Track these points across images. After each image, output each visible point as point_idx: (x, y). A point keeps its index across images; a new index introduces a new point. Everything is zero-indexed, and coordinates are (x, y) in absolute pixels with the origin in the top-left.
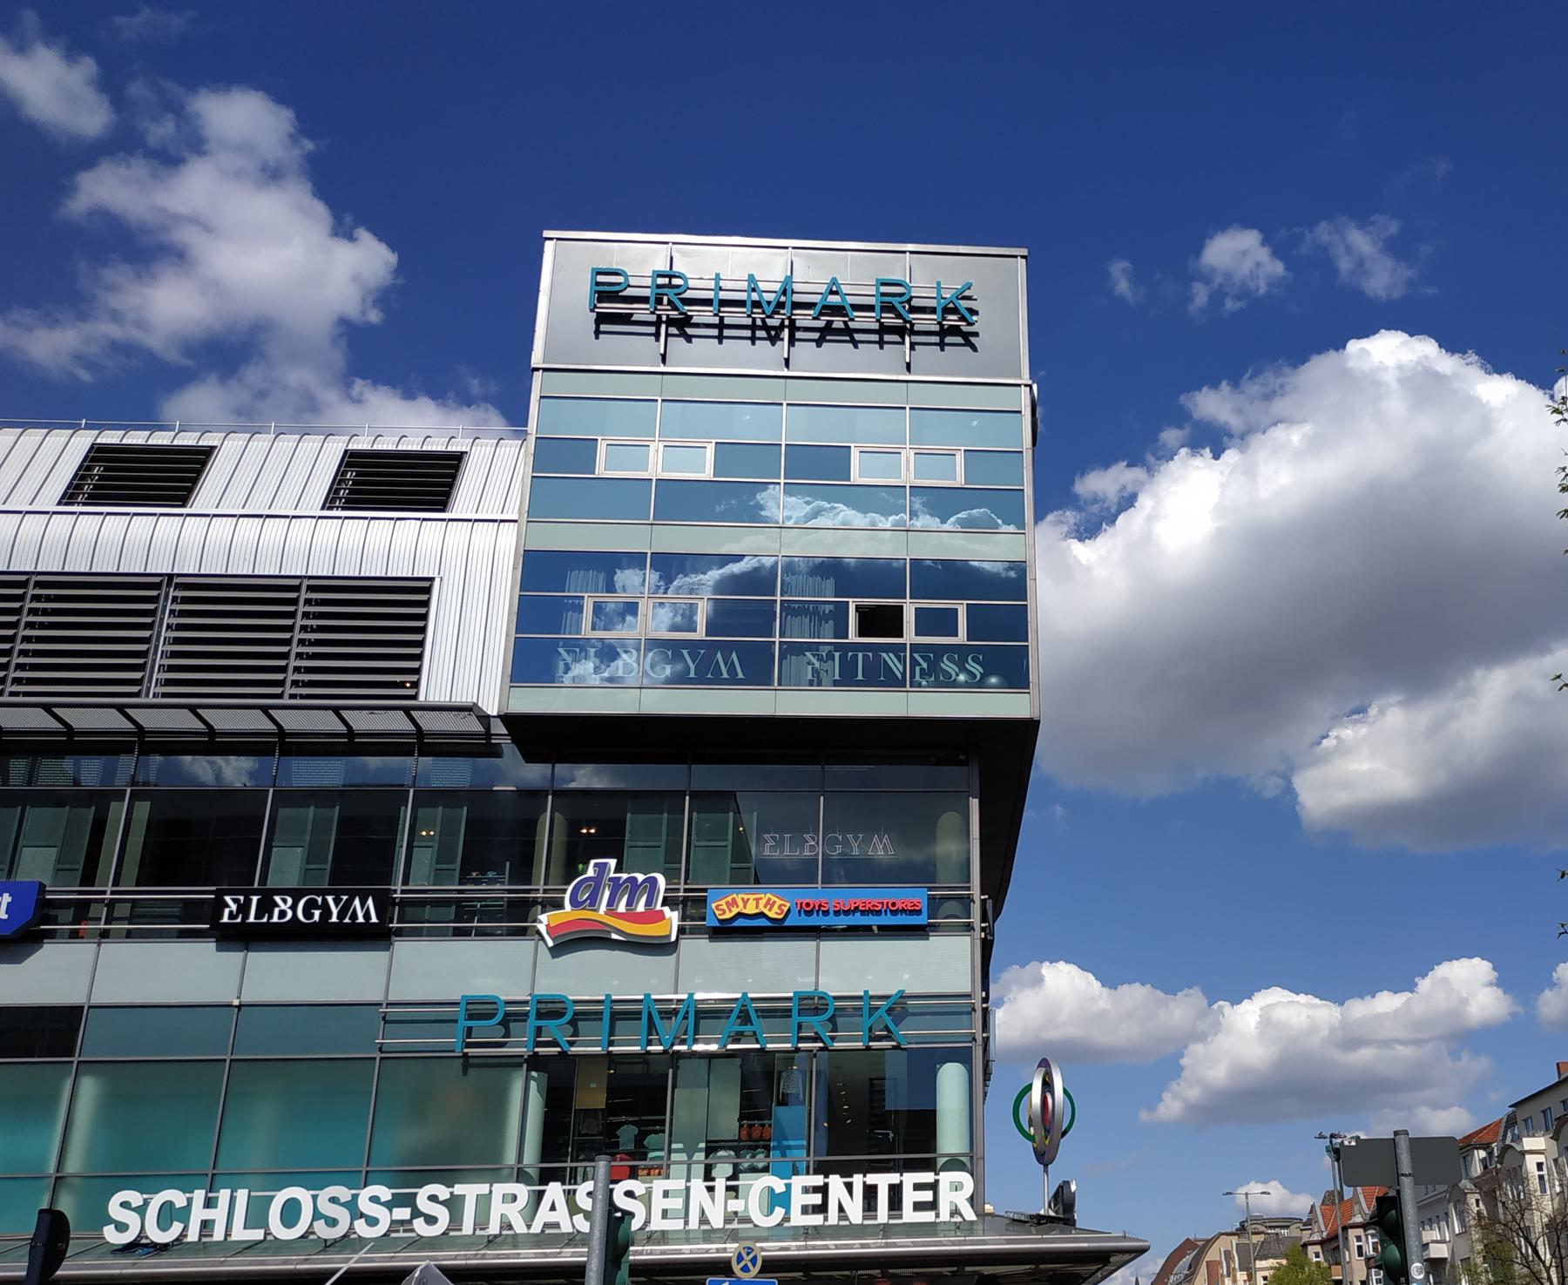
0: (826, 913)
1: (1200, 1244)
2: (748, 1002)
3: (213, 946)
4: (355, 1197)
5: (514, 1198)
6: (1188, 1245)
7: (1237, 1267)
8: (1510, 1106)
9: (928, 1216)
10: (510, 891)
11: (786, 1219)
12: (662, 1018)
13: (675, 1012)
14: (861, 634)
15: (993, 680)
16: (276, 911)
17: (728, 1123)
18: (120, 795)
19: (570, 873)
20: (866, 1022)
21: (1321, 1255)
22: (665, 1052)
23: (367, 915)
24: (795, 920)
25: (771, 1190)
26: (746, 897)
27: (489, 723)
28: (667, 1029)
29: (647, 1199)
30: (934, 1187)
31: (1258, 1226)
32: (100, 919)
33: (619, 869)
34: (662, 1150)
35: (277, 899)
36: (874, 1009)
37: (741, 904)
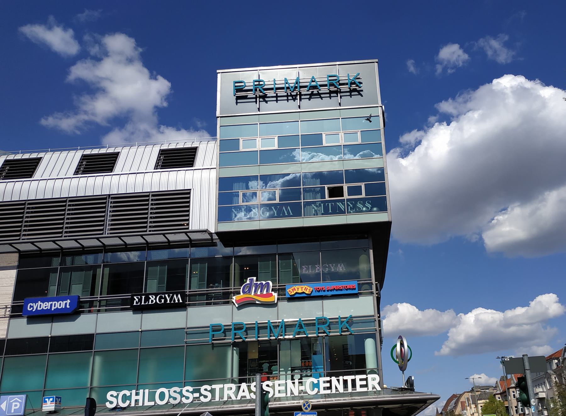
0: (324, 291)
1: (458, 396)
2: (301, 322)
3: (132, 312)
4: (181, 390)
5: (231, 389)
6: (454, 396)
7: (471, 403)
9: (365, 389)
11: (319, 392)
13: (278, 326)
14: (330, 197)
15: (375, 209)
16: (150, 300)
17: (298, 361)
19: (242, 282)
22: (276, 339)
23: (178, 300)
25: (313, 382)
26: (298, 287)
27: (212, 235)
28: (276, 331)
29: (273, 387)
30: (366, 379)
33: (257, 280)
35: (150, 296)
36: (342, 322)
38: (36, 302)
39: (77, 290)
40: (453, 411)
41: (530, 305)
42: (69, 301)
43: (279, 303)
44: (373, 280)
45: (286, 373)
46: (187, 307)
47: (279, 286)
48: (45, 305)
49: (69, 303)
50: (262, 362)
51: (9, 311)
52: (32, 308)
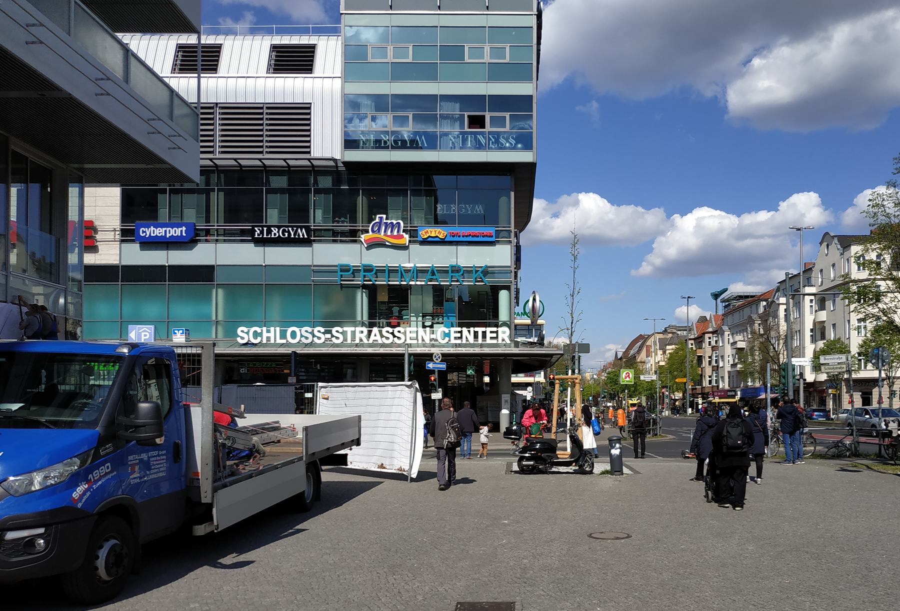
0: (459, 236)
1: (646, 336)
2: (434, 268)
3: (253, 245)
4: (313, 330)
6: (641, 337)
7: (658, 348)
9: (495, 341)
10: (350, 226)
11: (449, 340)
12: (405, 273)
13: (410, 270)
14: (469, 128)
15: (519, 146)
16: (273, 233)
17: (429, 307)
18: (213, 190)
19: (370, 220)
21: (694, 344)
22: (407, 284)
23: (303, 235)
24: (448, 239)
25: (444, 332)
26: (431, 230)
27: (337, 162)
28: (407, 276)
29: (405, 333)
30: (497, 332)
31: (673, 330)
32: (214, 235)
33: (387, 219)
34: (408, 316)
35: (272, 229)
36: (477, 271)
37: (430, 233)
38: (149, 227)
39: (190, 215)
40: (635, 357)
41: (779, 208)
42: (184, 228)
44: (512, 228)
45: (417, 319)
46: (313, 243)
48: (158, 231)
49: (185, 230)
50: (391, 305)
51: (119, 234)
52: (144, 234)
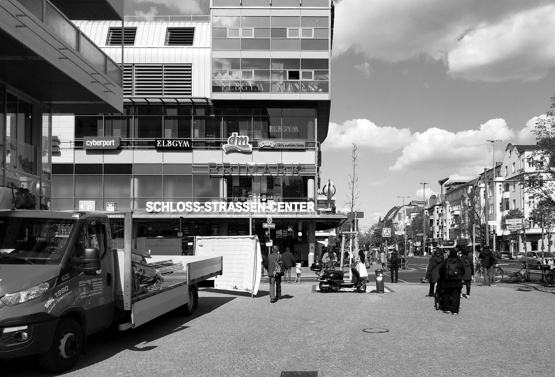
3: (156, 151)
4: (193, 204)
5: (223, 205)
8: (480, 175)
9: (305, 211)
11: (277, 210)
13: (253, 167)
14: (289, 79)
15: (320, 90)
16: (168, 144)
17: (265, 189)
19: (228, 136)
20: (292, 170)
23: (187, 145)
25: (274, 205)
30: (306, 205)
33: (239, 135)
35: (168, 141)
39: (117, 132)
40: (392, 220)
41: (480, 128)
42: (113, 141)
43: (254, 152)
44: (316, 141)
47: (253, 140)
50: (242, 188)
52: (89, 144)
